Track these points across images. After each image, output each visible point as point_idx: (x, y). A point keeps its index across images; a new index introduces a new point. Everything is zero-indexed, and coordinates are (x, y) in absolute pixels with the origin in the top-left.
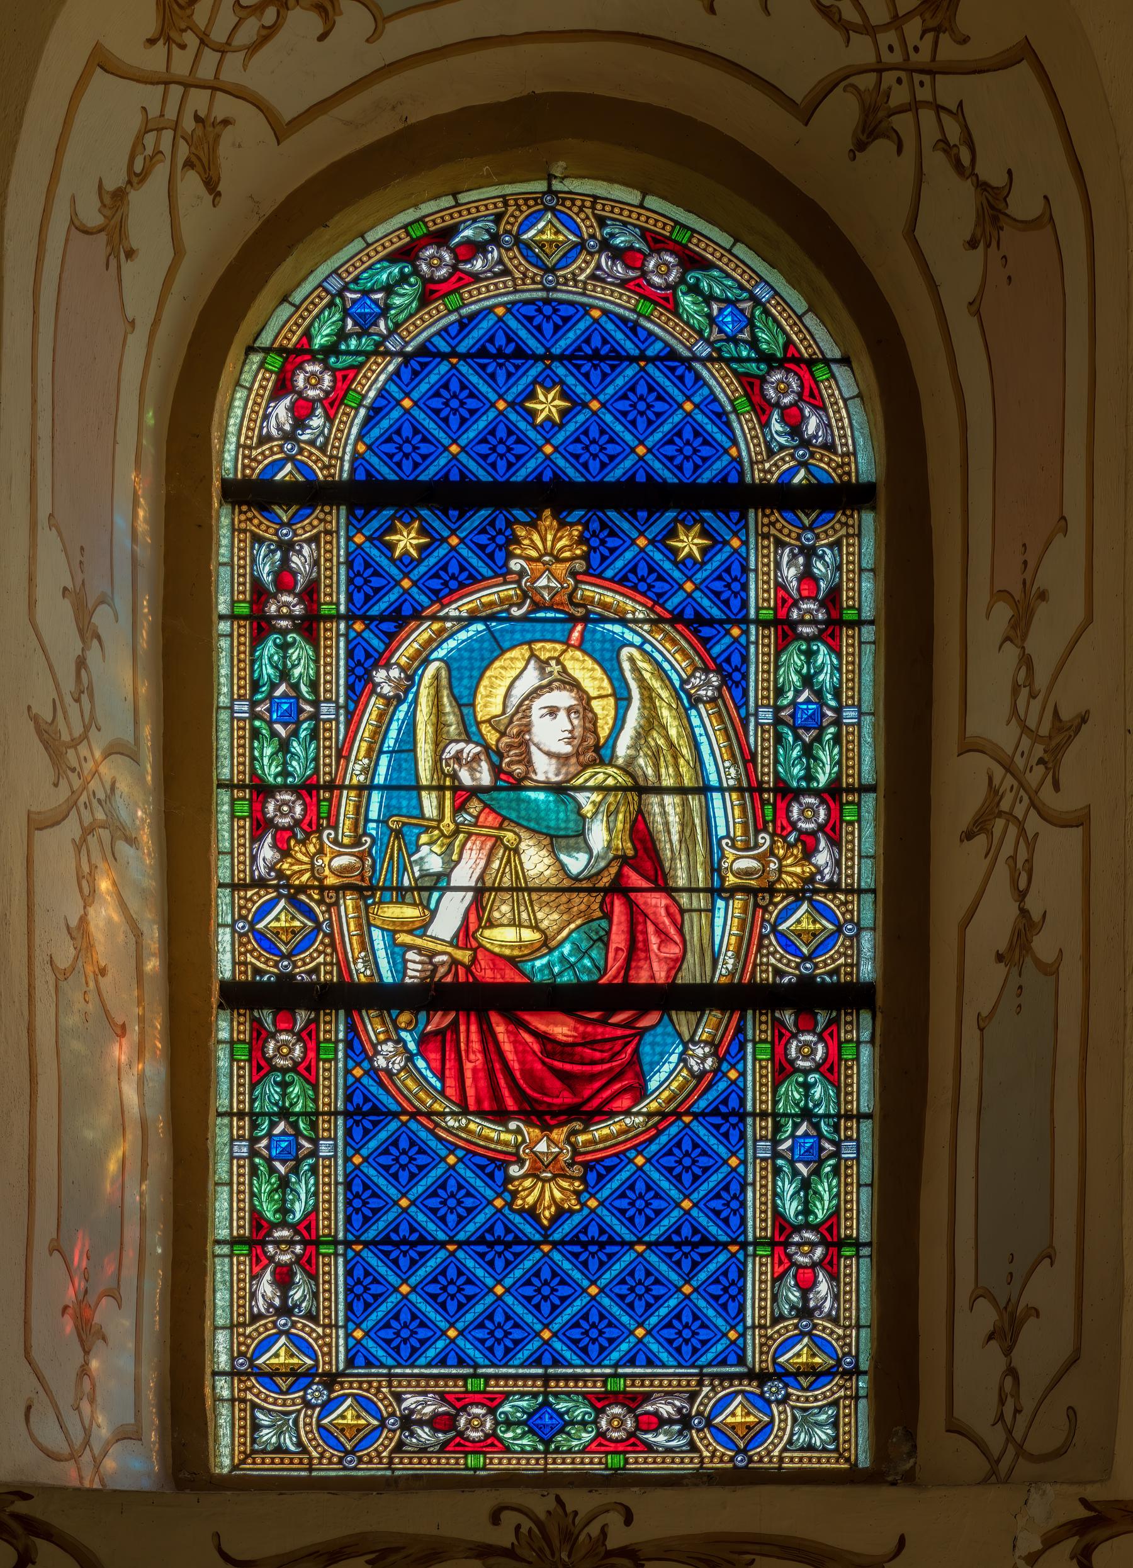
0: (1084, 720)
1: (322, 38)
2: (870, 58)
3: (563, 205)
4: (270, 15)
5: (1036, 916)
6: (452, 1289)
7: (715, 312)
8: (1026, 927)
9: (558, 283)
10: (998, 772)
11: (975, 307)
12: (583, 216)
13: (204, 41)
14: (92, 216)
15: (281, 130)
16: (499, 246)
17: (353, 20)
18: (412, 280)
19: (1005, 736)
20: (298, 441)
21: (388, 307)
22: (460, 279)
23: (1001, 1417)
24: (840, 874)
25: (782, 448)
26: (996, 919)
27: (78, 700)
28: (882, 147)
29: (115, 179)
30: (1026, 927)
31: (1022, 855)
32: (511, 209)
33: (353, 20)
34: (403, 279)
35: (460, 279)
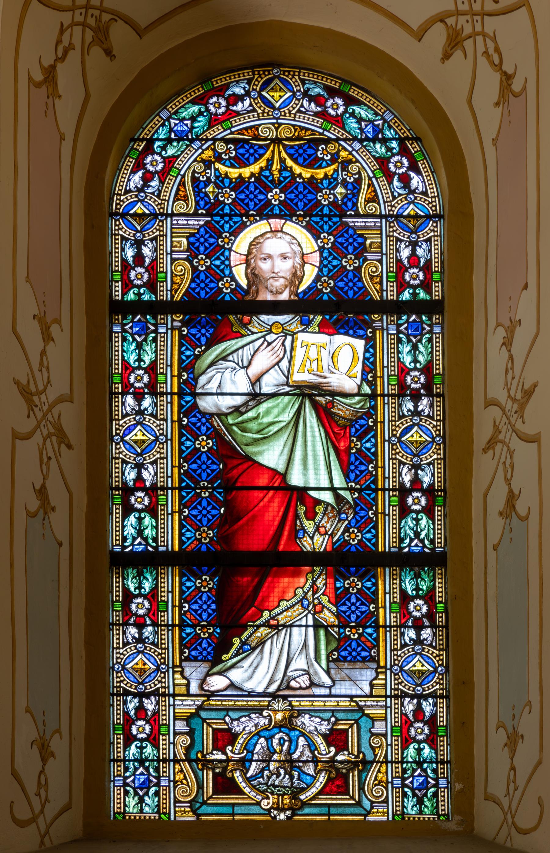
0: (536, 386)
3: (284, 74)
5: (516, 492)
6: (204, 467)
7: (363, 127)
8: (512, 499)
9: (281, 115)
12: (294, 80)
14: (39, 77)
16: (250, 97)
18: (205, 114)
19: (502, 396)
20: (145, 192)
21: (193, 127)
22: (230, 114)
24: (433, 412)
25: (400, 195)
26: (498, 500)
27: (38, 795)
28: (458, 54)
29: (48, 61)
30: (512, 499)
31: (508, 461)
32: (256, 77)
34: (200, 113)
35: (230, 114)
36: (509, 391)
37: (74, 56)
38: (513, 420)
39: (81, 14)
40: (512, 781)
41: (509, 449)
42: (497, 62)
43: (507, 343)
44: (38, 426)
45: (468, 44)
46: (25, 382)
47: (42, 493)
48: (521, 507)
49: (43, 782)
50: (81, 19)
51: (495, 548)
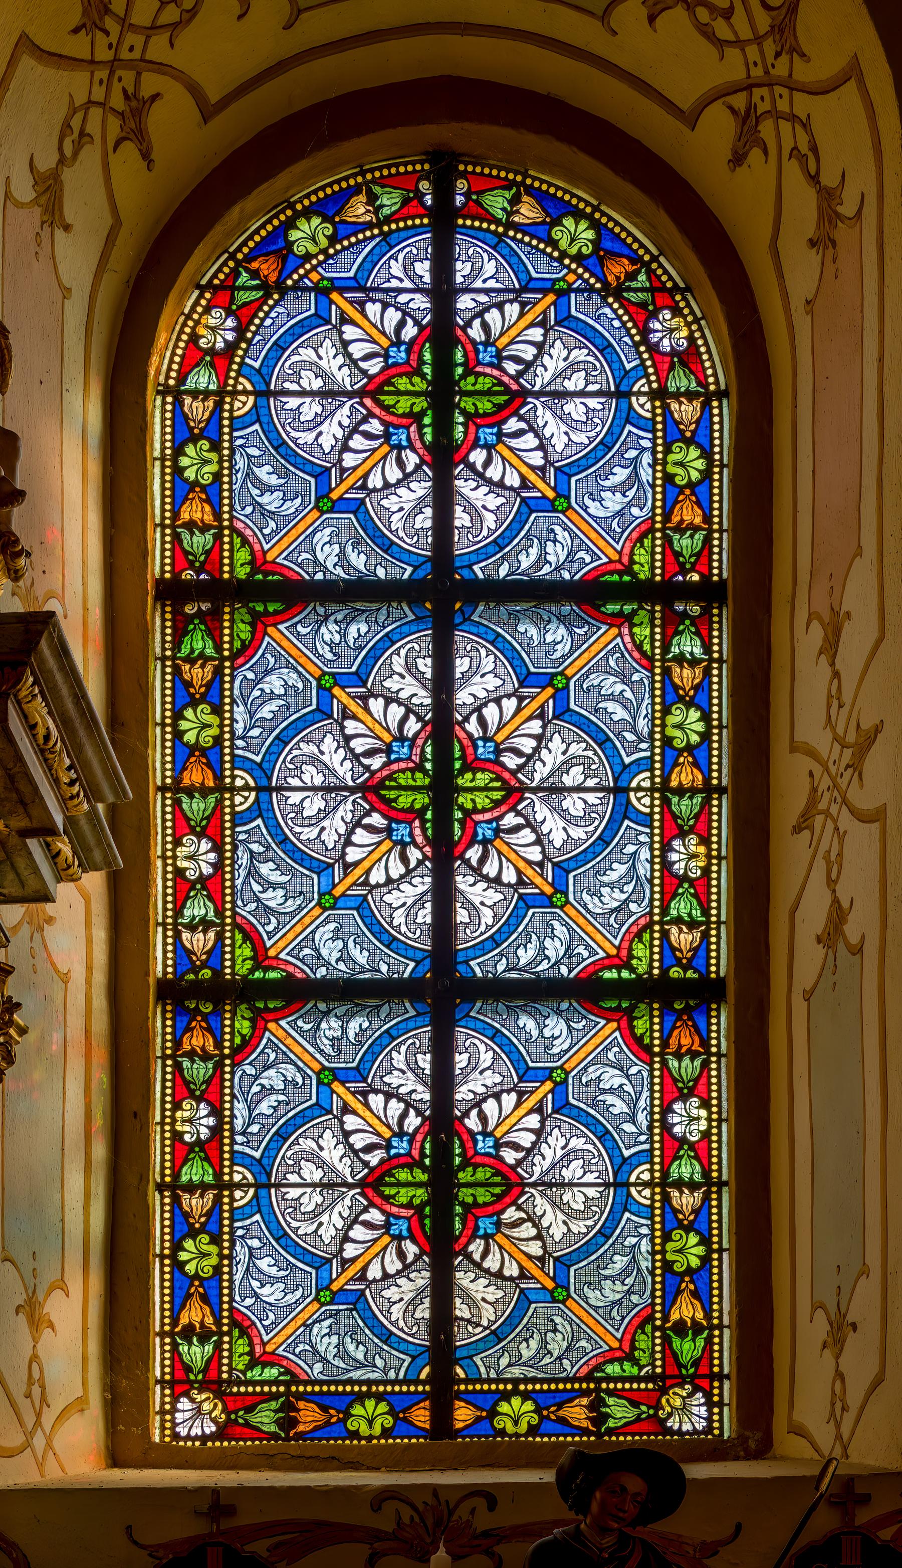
1: (240, 17)
2: (739, 74)
5: (845, 904)
8: (838, 915)
10: (818, 770)
11: (865, 1271)
15: (208, 112)
19: (822, 742)
23: (833, 1412)
26: (814, 915)
27: (28, 1396)
29: (47, 162)
30: (838, 915)
36: (838, 1426)
37: (91, 155)
38: (843, 782)
40: (837, 1404)
41: (834, 730)
43: (831, 646)
48: (852, 931)
49: (36, 1375)
51: (808, 996)
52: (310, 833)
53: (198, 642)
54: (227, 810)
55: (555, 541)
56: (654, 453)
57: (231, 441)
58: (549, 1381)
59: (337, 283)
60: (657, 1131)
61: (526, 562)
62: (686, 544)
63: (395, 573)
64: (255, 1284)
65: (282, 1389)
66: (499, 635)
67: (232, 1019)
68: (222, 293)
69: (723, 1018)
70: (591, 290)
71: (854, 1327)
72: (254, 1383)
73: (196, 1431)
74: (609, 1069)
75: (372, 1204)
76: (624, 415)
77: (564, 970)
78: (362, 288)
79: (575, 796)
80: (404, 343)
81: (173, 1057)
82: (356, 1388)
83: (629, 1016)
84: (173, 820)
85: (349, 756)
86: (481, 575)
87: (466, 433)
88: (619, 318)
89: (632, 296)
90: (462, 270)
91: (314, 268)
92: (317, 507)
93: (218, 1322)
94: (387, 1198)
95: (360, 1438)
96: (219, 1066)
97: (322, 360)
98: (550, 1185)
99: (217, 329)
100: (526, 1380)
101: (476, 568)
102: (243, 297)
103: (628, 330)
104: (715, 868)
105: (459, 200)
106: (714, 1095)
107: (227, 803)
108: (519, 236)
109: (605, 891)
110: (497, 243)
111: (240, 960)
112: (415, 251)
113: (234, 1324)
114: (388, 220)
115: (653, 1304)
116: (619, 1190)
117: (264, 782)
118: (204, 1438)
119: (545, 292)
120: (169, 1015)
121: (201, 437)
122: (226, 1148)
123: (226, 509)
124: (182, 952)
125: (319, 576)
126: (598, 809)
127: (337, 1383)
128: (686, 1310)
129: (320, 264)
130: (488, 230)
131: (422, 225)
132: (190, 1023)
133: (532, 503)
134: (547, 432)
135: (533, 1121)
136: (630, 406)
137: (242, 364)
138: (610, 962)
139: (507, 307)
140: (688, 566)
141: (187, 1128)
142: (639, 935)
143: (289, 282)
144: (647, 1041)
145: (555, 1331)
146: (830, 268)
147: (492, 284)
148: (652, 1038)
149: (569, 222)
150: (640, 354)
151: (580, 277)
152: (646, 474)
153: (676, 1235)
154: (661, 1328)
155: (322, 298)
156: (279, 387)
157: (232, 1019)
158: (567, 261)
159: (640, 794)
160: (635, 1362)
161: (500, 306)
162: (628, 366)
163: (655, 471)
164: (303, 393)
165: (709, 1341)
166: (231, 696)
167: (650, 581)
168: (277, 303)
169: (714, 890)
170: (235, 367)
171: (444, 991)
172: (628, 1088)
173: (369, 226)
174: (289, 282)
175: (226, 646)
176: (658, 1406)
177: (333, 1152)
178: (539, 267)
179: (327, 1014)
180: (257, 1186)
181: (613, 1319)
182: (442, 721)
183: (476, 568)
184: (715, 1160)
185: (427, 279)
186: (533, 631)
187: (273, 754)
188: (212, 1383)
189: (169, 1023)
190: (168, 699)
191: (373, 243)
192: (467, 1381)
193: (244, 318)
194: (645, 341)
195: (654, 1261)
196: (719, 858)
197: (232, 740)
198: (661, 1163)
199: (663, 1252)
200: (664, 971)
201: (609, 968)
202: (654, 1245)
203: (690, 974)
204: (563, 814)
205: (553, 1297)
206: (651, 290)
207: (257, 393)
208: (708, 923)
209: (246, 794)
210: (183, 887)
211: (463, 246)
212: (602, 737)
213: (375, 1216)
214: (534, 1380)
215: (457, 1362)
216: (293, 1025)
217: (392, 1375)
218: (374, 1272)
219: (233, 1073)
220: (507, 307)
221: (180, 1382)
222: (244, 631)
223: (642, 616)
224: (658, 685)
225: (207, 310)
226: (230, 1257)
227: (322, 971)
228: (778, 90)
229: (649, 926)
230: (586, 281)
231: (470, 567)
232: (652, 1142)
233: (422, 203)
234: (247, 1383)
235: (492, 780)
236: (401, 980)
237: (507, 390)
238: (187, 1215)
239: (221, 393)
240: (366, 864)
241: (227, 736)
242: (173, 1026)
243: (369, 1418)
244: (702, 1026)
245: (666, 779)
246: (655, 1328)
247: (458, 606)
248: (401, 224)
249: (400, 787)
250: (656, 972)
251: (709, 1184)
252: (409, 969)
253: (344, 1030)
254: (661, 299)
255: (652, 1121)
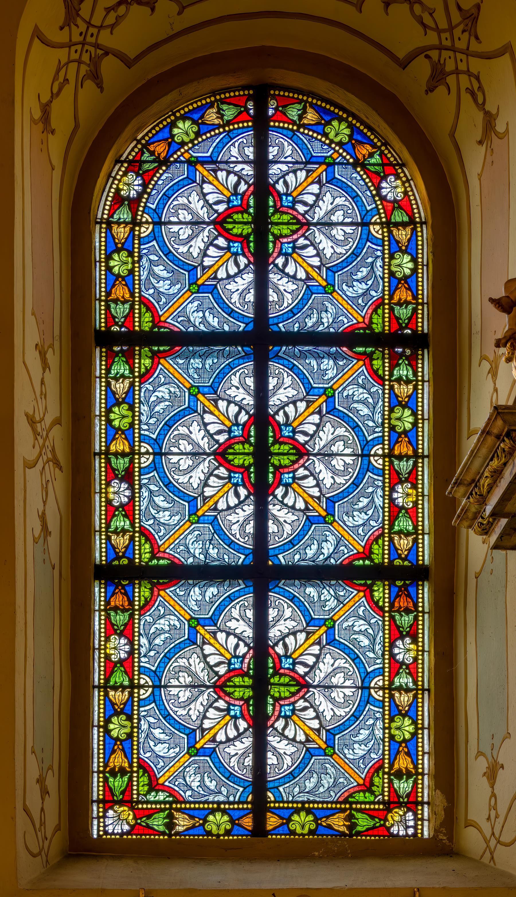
2: (436, 42)
4: (122, 9)
13: (89, 24)
17: (165, 6)
28: (441, 89)
29: (45, 99)
33: (165, 6)
37: (69, 90)
39: (76, 51)
42: (480, 101)
44: (40, 454)
45: (451, 80)
46: (31, 413)
47: (43, 517)
50: (75, 56)
52: (183, 249)
53: (120, 367)
54: (137, 465)
55: (326, 311)
56: (383, 259)
57: (140, 480)
58: (323, 803)
59: (200, 159)
60: (387, 657)
61: (310, 553)
62: (404, 313)
63: (234, 328)
64: (152, 743)
65: (168, 806)
66: (294, 365)
67: (140, 359)
68: (135, 165)
69: (426, 590)
70: (348, 163)
71: (502, 767)
72: (152, 803)
73: (118, 830)
74: (357, 618)
75: (220, 697)
76: (366, 467)
77: (332, 561)
78: (215, 162)
79: (339, 228)
80: (239, 194)
81: (105, 610)
82: (211, 806)
83: (370, 357)
84: (106, 471)
85: (207, 667)
86: (283, 330)
87: (274, 710)
88: (364, 180)
89: (372, 168)
90: (273, 152)
91: (187, 151)
92: (188, 753)
93: (131, 766)
94: (229, 694)
95: (212, 835)
96: (132, 616)
97: (193, 204)
98: (325, 455)
99: (131, 185)
100: (309, 802)
101: (281, 325)
102: (146, 166)
103: (369, 188)
104: (420, 502)
105: (271, 112)
106: (420, 717)
107: (137, 461)
108: (306, 132)
109: (356, 746)
110: (292, 136)
111: (143, 553)
112: (246, 372)
113: (140, 767)
114: (229, 123)
115: (384, 759)
116: (364, 228)
117: (157, 683)
118: (122, 834)
119: (320, 164)
120: (103, 586)
121: (122, 249)
122: (136, 664)
123: (137, 291)
124: (110, 545)
125: (191, 329)
126: (352, 698)
127: (199, 803)
128: (403, 763)
129: (190, 149)
130: (288, 128)
131: (248, 126)
132: (115, 590)
133: (312, 751)
134: (321, 709)
135: (316, 418)
136: (369, 231)
137: (145, 207)
138: (358, 556)
139: (299, 173)
140: (404, 633)
141: (112, 652)
142: (376, 540)
143: (172, 159)
144: (381, 604)
145: (326, 541)
146: (489, 159)
147: (289, 159)
148: (384, 602)
149: (335, 123)
150: (375, 202)
151: (341, 155)
152: (379, 733)
153: (397, 256)
154: (389, 774)
155: (191, 168)
156: (167, 220)
157: (140, 359)
158: (333, 146)
159: (376, 458)
160: (372, 793)
161: (295, 172)
162: (369, 208)
163: (384, 269)
164: (180, 223)
165: (415, 783)
166: (139, 632)
167: (382, 333)
168: (164, 171)
169: (420, 515)
170: (141, 209)
171: (261, 340)
172: (370, 631)
173: (219, 126)
174: (172, 159)
175: (137, 370)
176: (386, 820)
177: (197, 434)
178: (317, 150)
179: (194, 586)
180: (154, 687)
181: (359, 767)
182: (261, 265)
183: (280, 557)
184: (420, 408)
185: (251, 157)
186: (314, 363)
187: (163, 433)
188: (127, 800)
189: (103, 363)
190: (103, 440)
191: (222, 136)
192: (275, 802)
193: (147, 178)
194: (379, 194)
195: (384, 733)
196: (423, 381)
197: (139, 424)
198: (389, 676)
199: (390, 728)
200: (391, 561)
201: (358, 559)
202: (384, 723)
203: (406, 563)
204: (332, 701)
205: (325, 753)
206: (383, 165)
207: (154, 223)
208: (417, 381)
209: (147, 456)
210: (111, 511)
211: (274, 137)
212: (354, 194)
213: (221, 704)
214: (314, 802)
215: (268, 790)
216: (174, 592)
217: (231, 799)
218: (222, 274)
219: (139, 620)
220: (299, 173)
221: (108, 801)
222: (147, 362)
223: (378, 354)
224: (387, 396)
225: (125, 174)
226: (139, 728)
227: (191, 560)
228: (459, 56)
229: (382, 535)
230: (344, 158)
231: (277, 324)
232: (384, 664)
233: (249, 114)
234: (148, 802)
235: (291, 449)
236: (237, 566)
237: (298, 222)
238: (114, 393)
239: (132, 452)
240: (217, 413)
241: (137, 422)
242: (105, 592)
243: (218, 823)
244: (413, 595)
245: (391, 449)
246: (384, 773)
247: (271, 348)
248: (236, 126)
249: (235, 686)
250: (386, 561)
251: (416, 691)
252: (241, 561)
253: (204, 365)
254: (388, 169)
255: (384, 651)
